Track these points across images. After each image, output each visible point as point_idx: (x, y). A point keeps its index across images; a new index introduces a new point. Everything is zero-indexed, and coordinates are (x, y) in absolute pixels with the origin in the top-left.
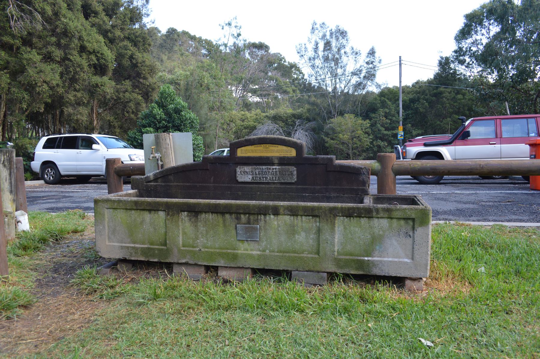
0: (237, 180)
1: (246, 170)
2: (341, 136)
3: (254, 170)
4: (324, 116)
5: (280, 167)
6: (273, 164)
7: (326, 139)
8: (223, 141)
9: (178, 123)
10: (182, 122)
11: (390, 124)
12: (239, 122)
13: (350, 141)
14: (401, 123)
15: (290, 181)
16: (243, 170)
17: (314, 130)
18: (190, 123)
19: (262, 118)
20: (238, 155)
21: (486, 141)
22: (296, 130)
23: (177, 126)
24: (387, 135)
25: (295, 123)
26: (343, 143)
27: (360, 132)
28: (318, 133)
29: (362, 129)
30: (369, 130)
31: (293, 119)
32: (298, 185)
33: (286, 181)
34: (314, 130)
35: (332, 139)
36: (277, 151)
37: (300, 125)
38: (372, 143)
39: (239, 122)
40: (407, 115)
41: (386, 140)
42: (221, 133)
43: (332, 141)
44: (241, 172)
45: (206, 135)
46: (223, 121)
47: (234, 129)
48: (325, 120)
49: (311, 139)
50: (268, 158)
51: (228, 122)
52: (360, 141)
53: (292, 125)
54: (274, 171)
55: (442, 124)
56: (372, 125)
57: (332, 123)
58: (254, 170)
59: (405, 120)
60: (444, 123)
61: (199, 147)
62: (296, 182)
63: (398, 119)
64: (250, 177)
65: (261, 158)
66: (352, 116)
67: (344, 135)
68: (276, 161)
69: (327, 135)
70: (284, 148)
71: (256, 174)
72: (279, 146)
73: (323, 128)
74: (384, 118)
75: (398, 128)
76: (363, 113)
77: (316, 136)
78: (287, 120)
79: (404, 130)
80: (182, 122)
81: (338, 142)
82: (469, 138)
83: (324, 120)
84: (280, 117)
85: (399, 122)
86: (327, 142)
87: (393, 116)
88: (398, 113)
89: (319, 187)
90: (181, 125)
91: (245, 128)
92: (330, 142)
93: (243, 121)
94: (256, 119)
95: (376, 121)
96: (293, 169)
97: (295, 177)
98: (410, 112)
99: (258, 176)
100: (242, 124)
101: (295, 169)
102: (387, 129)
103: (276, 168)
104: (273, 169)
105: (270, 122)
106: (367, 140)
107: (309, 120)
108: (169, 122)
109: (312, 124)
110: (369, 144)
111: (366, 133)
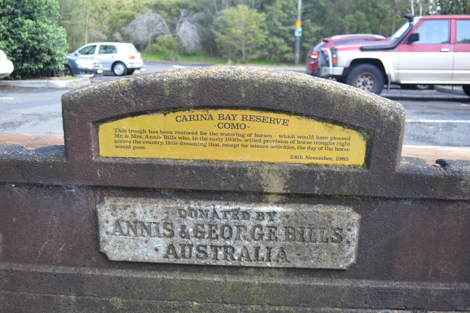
0: (104, 256)
1: (140, 216)
2: (233, 30)
3: (175, 219)
4: (214, 7)
5: (289, 209)
6: (260, 196)
7: (218, 34)
8: (94, 33)
9: (29, 9)
10: (35, 7)
11: (288, 18)
12: (114, 10)
13: (243, 37)
14: (299, 17)
15: (329, 265)
16: (126, 215)
17: (201, 22)
18: (46, 9)
19: (142, 6)
20: (103, 153)
21: (437, 48)
22: (181, 22)
23: (28, 13)
24: (284, 31)
25: (179, 12)
26: (235, 39)
27: (254, 26)
28: (206, 26)
29: (257, 23)
30: (265, 25)
31: (178, 8)
32: (359, 278)
33: (311, 264)
34: (201, 22)
35: (223, 33)
36: (283, 143)
37: (185, 16)
38: (267, 39)
39: (114, 10)
40: (306, 9)
41: (282, 37)
42: (92, 23)
43: (223, 36)
44: (117, 223)
45: (72, 25)
46: (93, 8)
47: (108, 18)
48: (214, 11)
49: (198, 32)
50: (238, 171)
51: (101, 9)
52: (254, 36)
53: (176, 16)
54: (265, 223)
55: (343, 20)
56: (269, 19)
57: (223, 14)
58: (175, 219)
59: (304, 14)
60: (346, 20)
61: (60, 42)
62: (352, 267)
63: (297, 13)
64: (161, 244)
65: (205, 170)
66: (246, 7)
67: (236, 29)
68: (276, 185)
69: (217, 28)
70: (316, 128)
71: (184, 233)
72: (293, 119)
73: (212, 21)
74: (281, 12)
75: (295, 23)
76: (258, 4)
77: (204, 29)
78: (170, 10)
79: (303, 26)
80: (35, 7)
81: (230, 38)
82: (415, 43)
83: (214, 11)
84: (162, 6)
85: (296, 17)
86: (217, 37)
87: (291, 9)
88: (297, 6)
89: (442, 287)
90: (34, 12)
91: (122, 17)
92: (220, 37)
93: (119, 9)
94: (135, 7)
95: (272, 15)
96: (348, 219)
97: (352, 249)
98: (309, 5)
99: (193, 240)
100: (118, 12)
101: (356, 217)
102: (284, 24)
103: (272, 214)
104: (260, 215)
105: (151, 11)
106: (262, 36)
107: (196, 10)
108: (16, 7)
109: (200, 15)
110: (264, 40)
111: (262, 28)
